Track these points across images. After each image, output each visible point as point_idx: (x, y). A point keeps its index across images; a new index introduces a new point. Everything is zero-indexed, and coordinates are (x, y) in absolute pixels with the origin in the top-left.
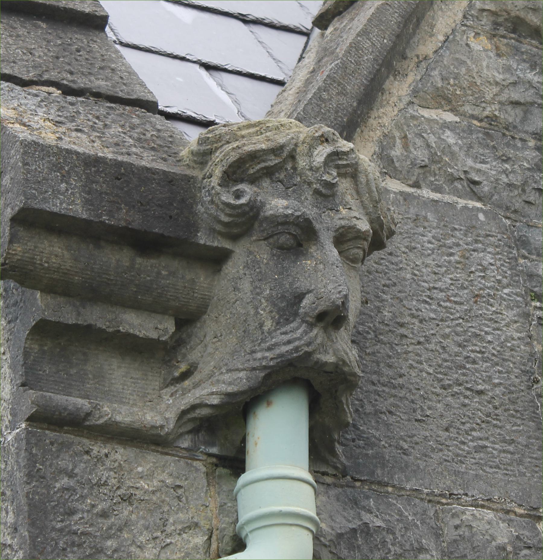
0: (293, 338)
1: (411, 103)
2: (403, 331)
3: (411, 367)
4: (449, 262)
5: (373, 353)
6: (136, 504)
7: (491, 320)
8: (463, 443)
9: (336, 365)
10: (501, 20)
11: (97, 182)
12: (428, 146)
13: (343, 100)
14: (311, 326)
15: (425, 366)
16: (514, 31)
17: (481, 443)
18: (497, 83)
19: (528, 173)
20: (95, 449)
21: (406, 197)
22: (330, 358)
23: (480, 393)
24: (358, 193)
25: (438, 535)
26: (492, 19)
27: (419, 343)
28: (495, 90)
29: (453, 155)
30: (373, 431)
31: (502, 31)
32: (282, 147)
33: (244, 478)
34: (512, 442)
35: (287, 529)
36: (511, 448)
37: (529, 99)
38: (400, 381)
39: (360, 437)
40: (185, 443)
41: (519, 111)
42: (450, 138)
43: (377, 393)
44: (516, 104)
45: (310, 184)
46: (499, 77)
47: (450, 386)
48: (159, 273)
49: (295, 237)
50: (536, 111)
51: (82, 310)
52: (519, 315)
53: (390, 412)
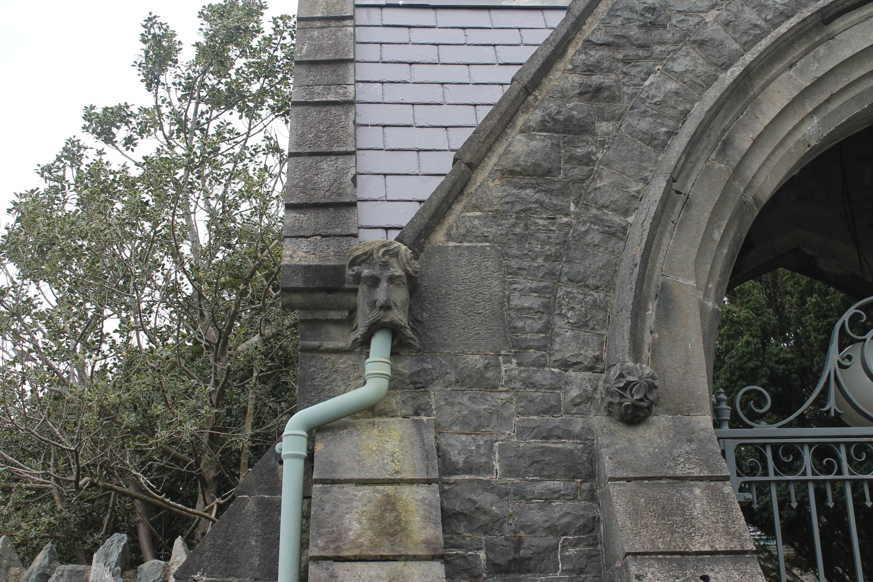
0: (375, 315)
13: (422, 220)
21: (456, 247)
22: (388, 320)
25: (456, 367)
32: (367, 252)
33: (368, 360)
40: (358, 350)
41: (510, 205)
42: (476, 222)
44: (508, 203)
46: (500, 194)
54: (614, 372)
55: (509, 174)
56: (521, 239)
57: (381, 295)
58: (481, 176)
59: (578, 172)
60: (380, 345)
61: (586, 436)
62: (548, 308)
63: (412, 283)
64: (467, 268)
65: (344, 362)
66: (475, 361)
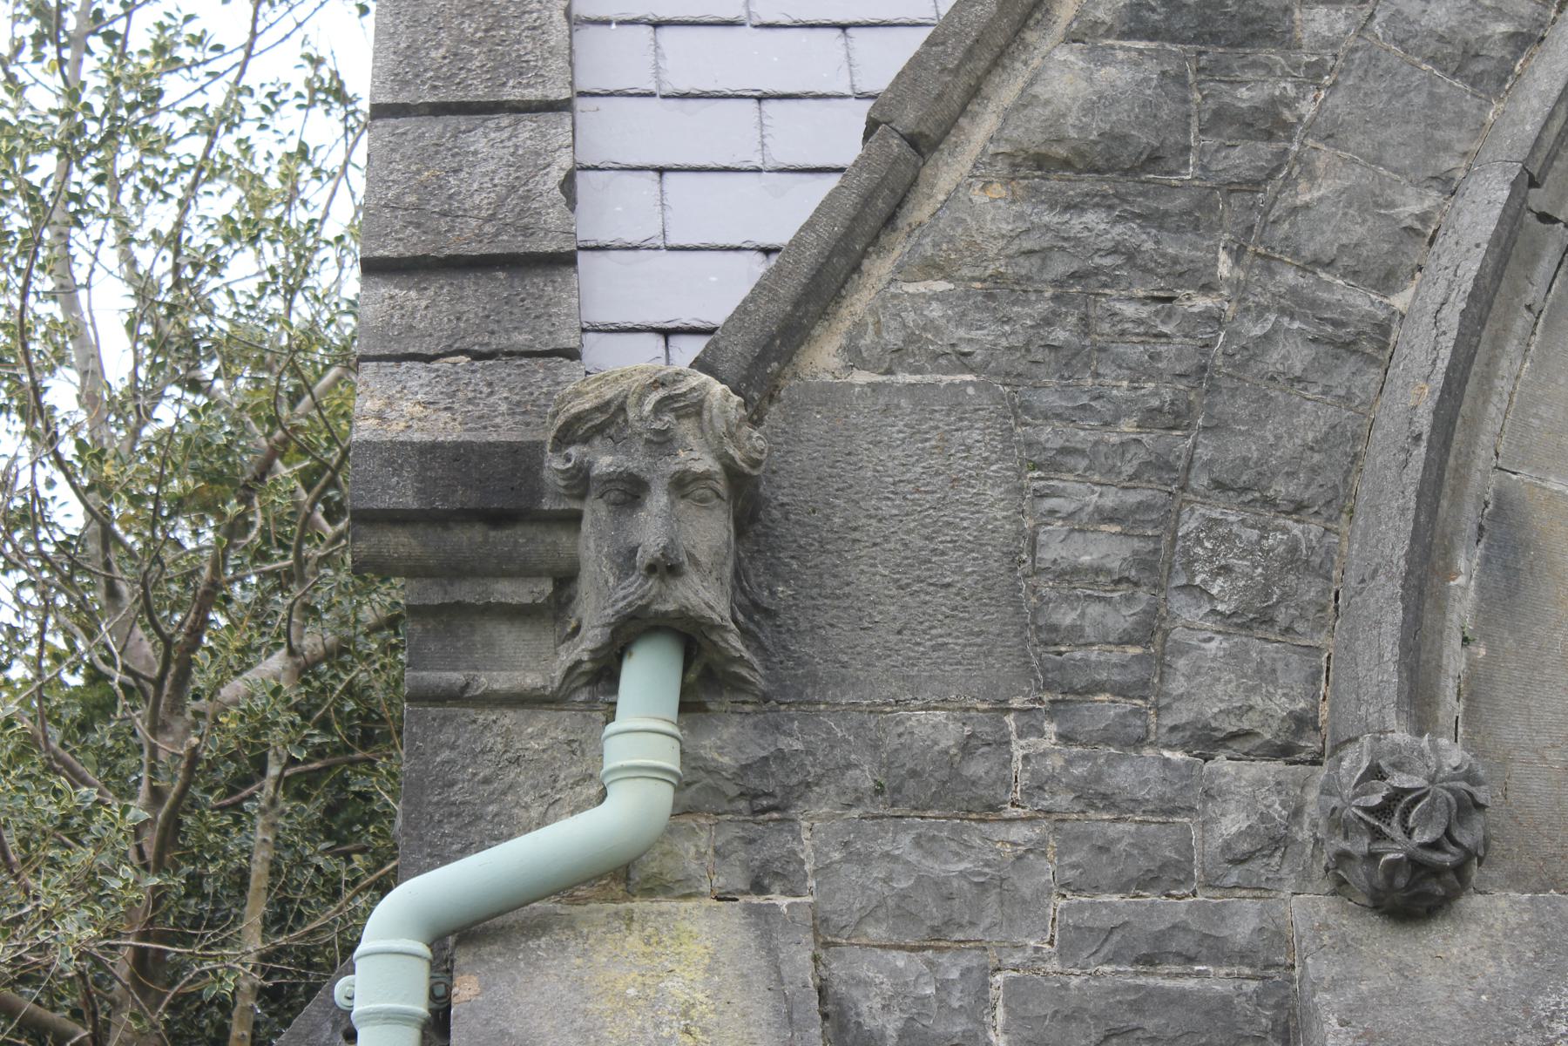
0: (634, 590)
1: (893, 280)
2: (856, 535)
3: (862, 572)
4: (923, 449)
5: (816, 566)
6: (524, 765)
7: (969, 504)
8: (919, 644)
9: (680, 611)
10: (1019, 160)
11: (433, 469)
12: (905, 326)
14: (647, 578)
15: (880, 569)
16: (1039, 168)
17: (940, 640)
18: (1003, 236)
19: (1031, 331)
20: (481, 719)
22: (671, 607)
23: (948, 585)
24: (702, 431)
25: (875, 746)
26: (1007, 161)
27: (875, 545)
28: (1001, 243)
29: (938, 331)
30: (807, 649)
31: (1023, 171)
32: (608, 403)
33: (611, 728)
34: (978, 634)
35: (631, 782)
36: (979, 640)
37: (1045, 245)
38: (847, 589)
39: (789, 658)
40: (582, 696)
42: (935, 311)
43: (816, 607)
44: (1030, 253)
45: (640, 434)
47: (908, 585)
48: (516, 542)
49: (624, 492)
50: (1056, 255)
51: (449, 588)
52: (1008, 491)
53: (832, 625)
54: (1353, 762)
55: (1034, 164)
56: (1069, 360)
57: (651, 529)
58: (948, 173)
59: (1241, 158)
60: (649, 681)
61: (1270, 958)
62: (1151, 570)
63: (745, 496)
64: (905, 447)
65: (538, 733)
66: (934, 728)
